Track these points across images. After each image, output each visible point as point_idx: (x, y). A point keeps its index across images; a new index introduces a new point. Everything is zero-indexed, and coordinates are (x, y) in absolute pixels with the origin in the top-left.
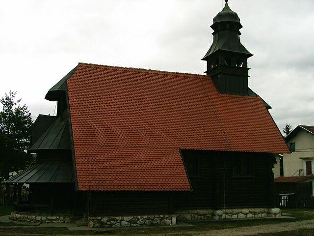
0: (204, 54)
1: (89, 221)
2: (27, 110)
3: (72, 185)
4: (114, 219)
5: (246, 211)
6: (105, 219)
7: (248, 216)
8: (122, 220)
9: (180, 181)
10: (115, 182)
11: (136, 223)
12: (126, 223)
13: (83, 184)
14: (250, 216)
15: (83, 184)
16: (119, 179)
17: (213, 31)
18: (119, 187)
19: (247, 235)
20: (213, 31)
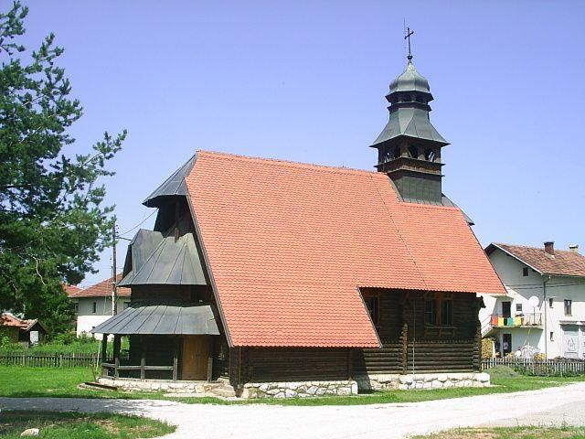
0: (374, 139)
1: (94, 176)
2: (58, 62)
3: (221, 338)
4: (276, 387)
5: (442, 376)
6: (264, 386)
7: (413, 386)
8: (286, 389)
9: (363, 333)
10: (279, 333)
11: (305, 392)
12: (293, 393)
13: (237, 338)
14: (448, 384)
15: (237, 338)
16: (284, 331)
17: (390, 104)
18: (285, 341)
19: (570, 437)
20: (390, 104)
